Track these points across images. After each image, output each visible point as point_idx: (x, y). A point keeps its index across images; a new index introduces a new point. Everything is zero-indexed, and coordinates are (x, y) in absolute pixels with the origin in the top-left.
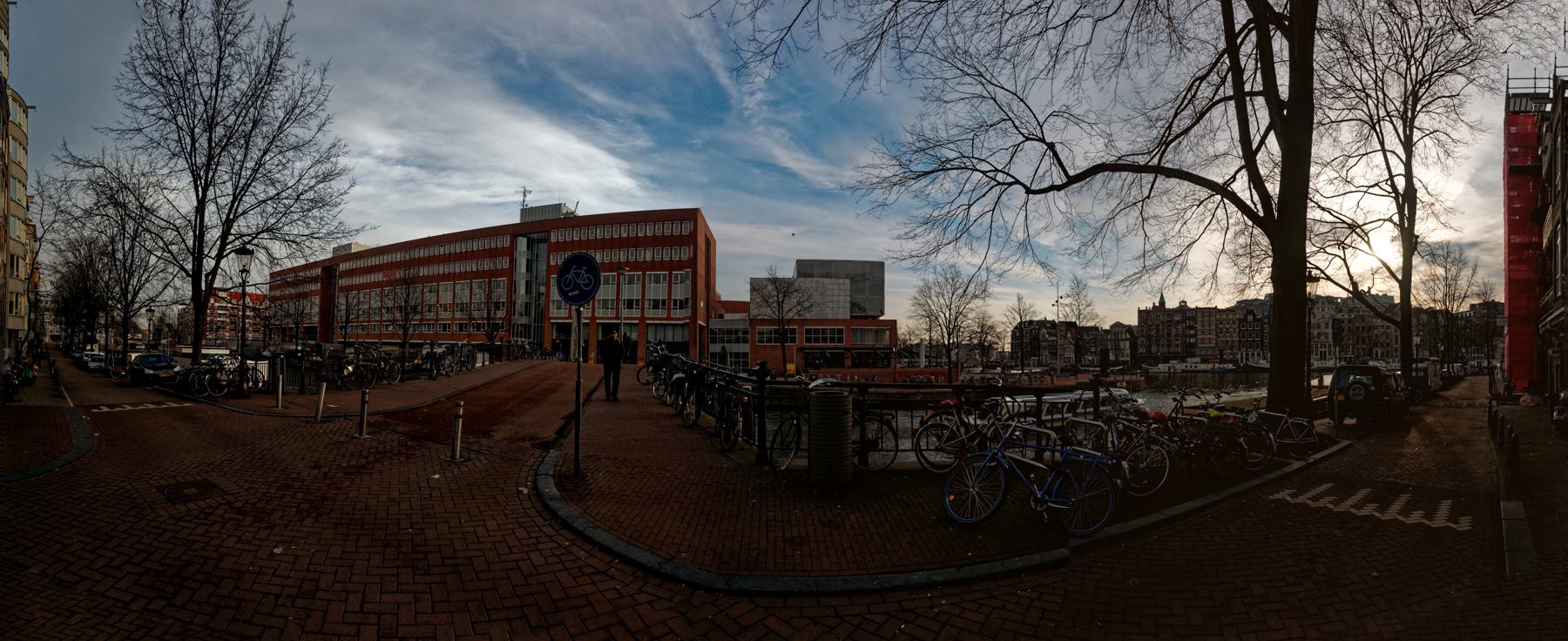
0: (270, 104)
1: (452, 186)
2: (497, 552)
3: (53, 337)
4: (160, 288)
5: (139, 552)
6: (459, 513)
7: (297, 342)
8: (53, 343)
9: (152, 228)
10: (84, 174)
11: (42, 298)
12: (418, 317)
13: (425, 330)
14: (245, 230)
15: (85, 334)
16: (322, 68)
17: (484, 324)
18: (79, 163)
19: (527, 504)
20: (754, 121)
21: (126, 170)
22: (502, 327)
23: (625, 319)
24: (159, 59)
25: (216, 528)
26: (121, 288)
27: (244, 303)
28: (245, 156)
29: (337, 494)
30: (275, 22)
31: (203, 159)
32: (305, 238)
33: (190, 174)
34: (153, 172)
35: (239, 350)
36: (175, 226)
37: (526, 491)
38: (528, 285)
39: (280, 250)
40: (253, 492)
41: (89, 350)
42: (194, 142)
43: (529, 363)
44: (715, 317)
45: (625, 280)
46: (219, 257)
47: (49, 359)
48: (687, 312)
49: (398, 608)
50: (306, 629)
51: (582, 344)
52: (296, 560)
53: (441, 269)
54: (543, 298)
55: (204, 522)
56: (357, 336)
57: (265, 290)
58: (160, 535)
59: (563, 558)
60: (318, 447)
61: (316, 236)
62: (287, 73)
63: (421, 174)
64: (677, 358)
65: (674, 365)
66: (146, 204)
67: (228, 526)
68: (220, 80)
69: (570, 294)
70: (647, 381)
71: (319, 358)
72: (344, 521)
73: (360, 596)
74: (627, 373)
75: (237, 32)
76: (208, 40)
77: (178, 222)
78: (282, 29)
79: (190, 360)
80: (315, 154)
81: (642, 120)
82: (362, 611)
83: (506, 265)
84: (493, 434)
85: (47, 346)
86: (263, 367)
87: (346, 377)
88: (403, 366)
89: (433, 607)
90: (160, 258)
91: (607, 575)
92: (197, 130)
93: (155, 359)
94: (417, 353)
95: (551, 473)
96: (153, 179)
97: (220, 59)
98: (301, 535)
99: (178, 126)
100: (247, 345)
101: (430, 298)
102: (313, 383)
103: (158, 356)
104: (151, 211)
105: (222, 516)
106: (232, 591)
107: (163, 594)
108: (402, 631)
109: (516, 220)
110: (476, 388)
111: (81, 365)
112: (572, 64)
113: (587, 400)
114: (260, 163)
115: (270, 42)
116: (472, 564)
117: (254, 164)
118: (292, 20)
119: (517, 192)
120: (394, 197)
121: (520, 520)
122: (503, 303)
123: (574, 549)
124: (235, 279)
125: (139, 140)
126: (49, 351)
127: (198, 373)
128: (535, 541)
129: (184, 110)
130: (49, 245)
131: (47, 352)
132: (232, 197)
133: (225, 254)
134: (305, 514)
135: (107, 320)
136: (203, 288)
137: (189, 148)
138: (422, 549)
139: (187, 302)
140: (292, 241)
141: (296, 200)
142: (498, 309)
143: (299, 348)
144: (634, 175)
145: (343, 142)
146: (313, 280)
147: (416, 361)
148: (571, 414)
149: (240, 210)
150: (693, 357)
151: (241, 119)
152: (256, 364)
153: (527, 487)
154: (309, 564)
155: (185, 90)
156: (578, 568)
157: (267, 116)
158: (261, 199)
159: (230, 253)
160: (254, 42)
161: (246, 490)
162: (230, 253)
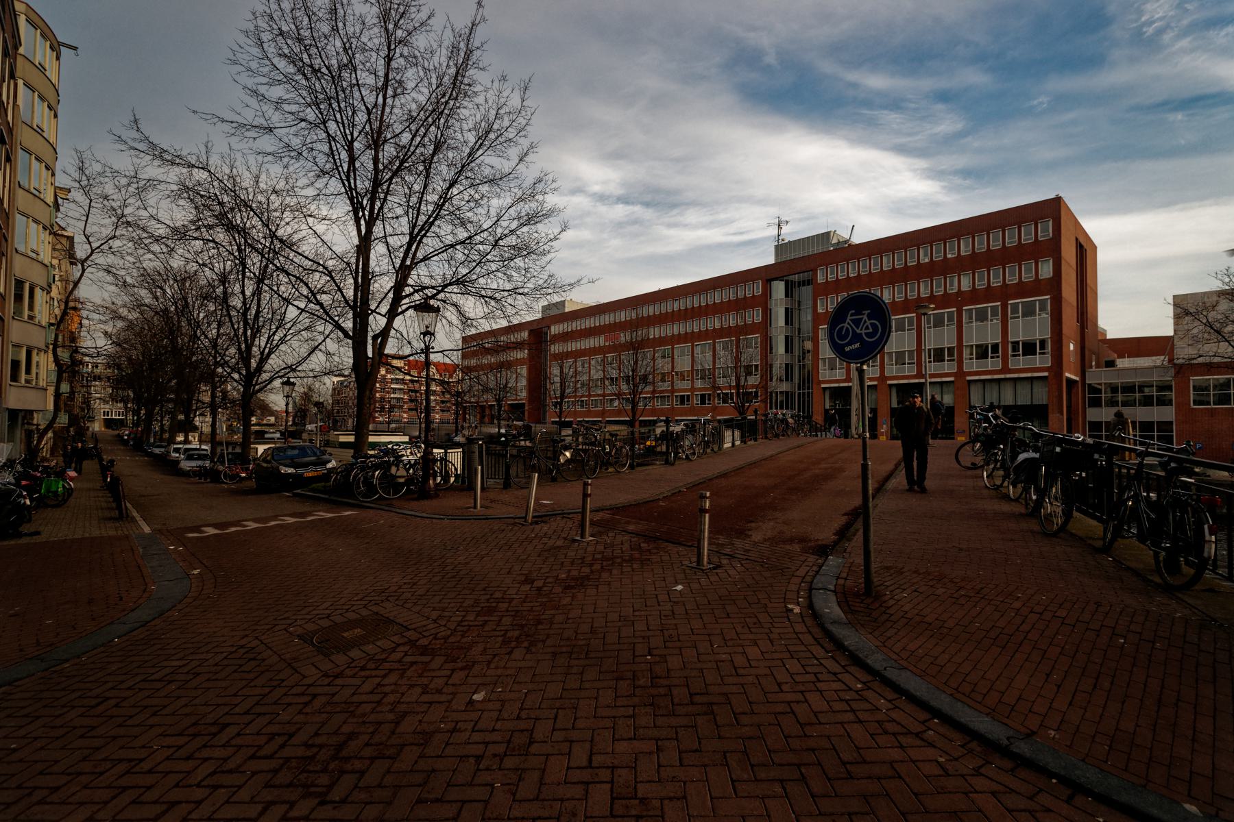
0: (457, 124)
1: (685, 226)
2: (762, 689)
3: (109, 423)
4: (304, 351)
5: (272, 736)
6: (709, 635)
7: (499, 424)
8: (110, 432)
9: (291, 268)
10: (174, 174)
11: (87, 359)
12: (649, 388)
13: (658, 404)
14: (427, 281)
15: (173, 418)
16: (522, 85)
17: (732, 394)
18: (159, 154)
19: (800, 628)
20: (1167, 37)
21: (247, 181)
22: (756, 396)
23: (932, 376)
24: (300, 40)
25: (392, 678)
26: (239, 349)
27: (428, 375)
28: (425, 186)
29: (554, 615)
30: (462, 23)
31: (367, 183)
32: (506, 294)
33: (348, 202)
34: (291, 191)
35: (423, 436)
36: (326, 268)
37: (797, 610)
38: (789, 342)
39: (475, 308)
40: (444, 623)
41: (180, 443)
42: (352, 160)
43: (793, 441)
44: (1098, 366)
45: (929, 322)
46: (392, 314)
47: (101, 460)
48: (1042, 361)
49: (636, 759)
50: (518, 796)
51: (868, 414)
52: (503, 706)
53: (676, 329)
54: (810, 357)
55: (374, 673)
56: (575, 414)
57: (456, 358)
58: (306, 704)
59: (855, 705)
60: (529, 556)
61: (521, 291)
62: (478, 88)
63: (647, 214)
64: (1024, 429)
65: (1018, 440)
66: (280, 233)
67: (409, 673)
68: (388, 85)
69: (847, 349)
70: (972, 464)
71: (528, 443)
72: (564, 649)
73: (588, 745)
74: (939, 453)
75: (411, 28)
76: (372, 32)
77: (330, 263)
78: (470, 33)
79: (352, 451)
80: (516, 190)
81: (944, 97)
82: (590, 766)
83: (758, 318)
84: (750, 533)
85: (95, 437)
86: (456, 457)
87: (563, 465)
88: (632, 449)
89: (680, 759)
90: (303, 310)
91: (922, 739)
92: (356, 144)
93: (296, 452)
94: (649, 432)
95: (832, 587)
96: (292, 201)
97: (389, 59)
98: (509, 672)
99: (329, 135)
100: (434, 429)
101: (663, 365)
102: (522, 475)
103: (302, 449)
104: (287, 244)
105: (400, 661)
106: (416, 762)
107: (312, 789)
108: (642, 790)
109: (771, 260)
110: (724, 475)
111: (169, 466)
112: (838, 50)
113: (878, 490)
114: (445, 198)
115: (455, 49)
116: (730, 703)
117: (438, 197)
118: (483, 24)
119: (769, 225)
120: (616, 242)
121: (791, 648)
122: (756, 366)
123: (869, 694)
124: (414, 343)
125: (267, 143)
126: (100, 445)
127: (363, 469)
128: (814, 679)
129: (338, 116)
130: (101, 274)
131: (95, 447)
132: (408, 238)
133: (400, 310)
134: (514, 644)
135: (213, 396)
136: (370, 354)
137: (345, 167)
138: (665, 682)
139: (346, 373)
140: (490, 298)
141: (494, 246)
142: (750, 374)
143: (503, 431)
144: (935, 174)
145: (550, 177)
146: (518, 346)
147: (648, 443)
148: (856, 509)
149: (420, 255)
150: (1058, 424)
151: (418, 139)
152: (446, 453)
153: (798, 604)
154: (521, 709)
155: (339, 88)
156: (878, 722)
157: (452, 139)
158: (447, 242)
159: (407, 309)
160: (435, 46)
161: (435, 621)
162: (407, 309)
